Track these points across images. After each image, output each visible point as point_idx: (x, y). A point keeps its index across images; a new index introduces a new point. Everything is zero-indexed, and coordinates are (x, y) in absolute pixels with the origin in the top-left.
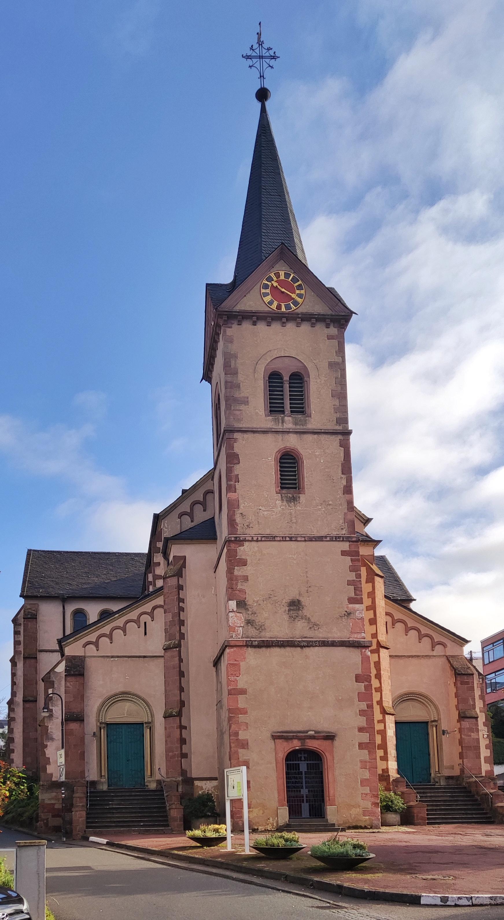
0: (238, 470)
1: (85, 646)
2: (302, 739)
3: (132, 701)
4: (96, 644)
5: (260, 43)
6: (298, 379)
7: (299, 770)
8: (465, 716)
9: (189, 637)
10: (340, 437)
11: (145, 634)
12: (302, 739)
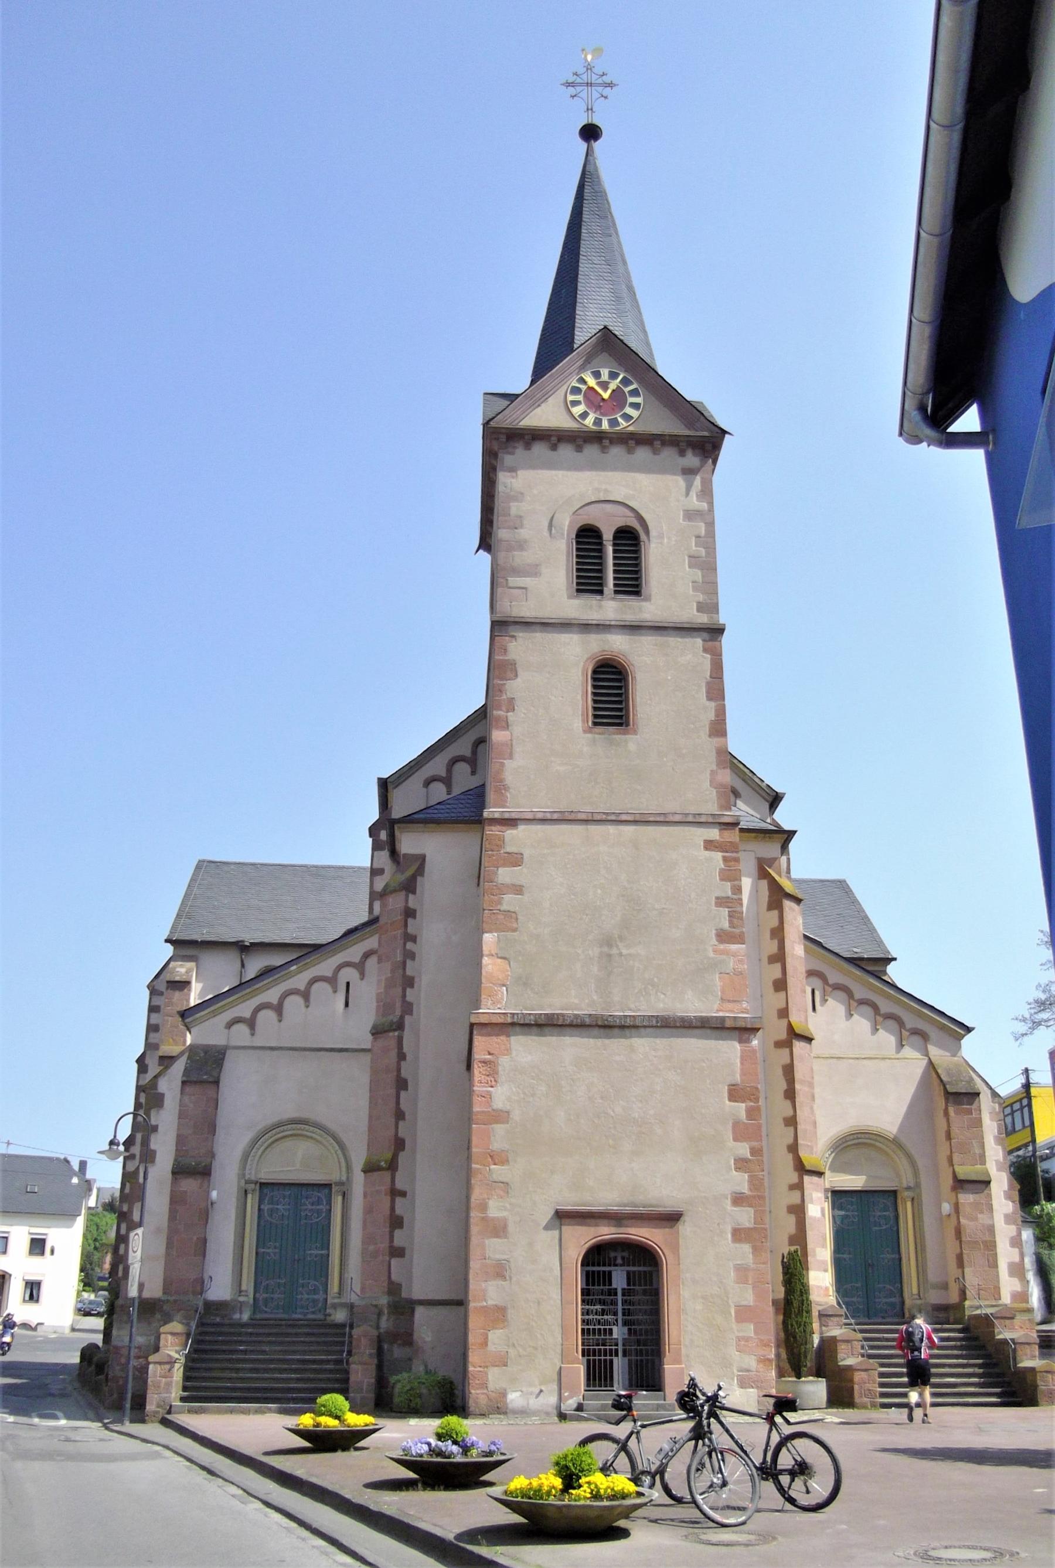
1: (229, 1025)
3: (311, 1138)
4: (251, 1023)
6: (629, 539)
7: (610, 1284)
11: (347, 1005)
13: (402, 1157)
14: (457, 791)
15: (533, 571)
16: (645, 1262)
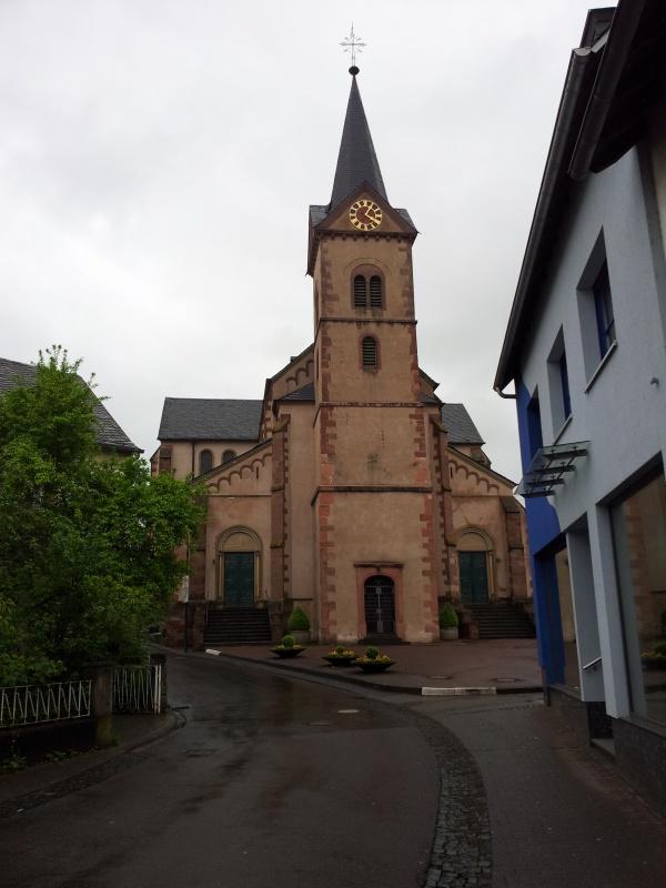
0: (330, 350)
2: (378, 568)
4: (218, 486)
5: (352, 35)
6: (377, 280)
8: (513, 547)
9: (291, 481)
10: (408, 326)
12: (378, 568)
13: (286, 542)
14: (301, 385)
15: (336, 298)
16: (388, 583)
